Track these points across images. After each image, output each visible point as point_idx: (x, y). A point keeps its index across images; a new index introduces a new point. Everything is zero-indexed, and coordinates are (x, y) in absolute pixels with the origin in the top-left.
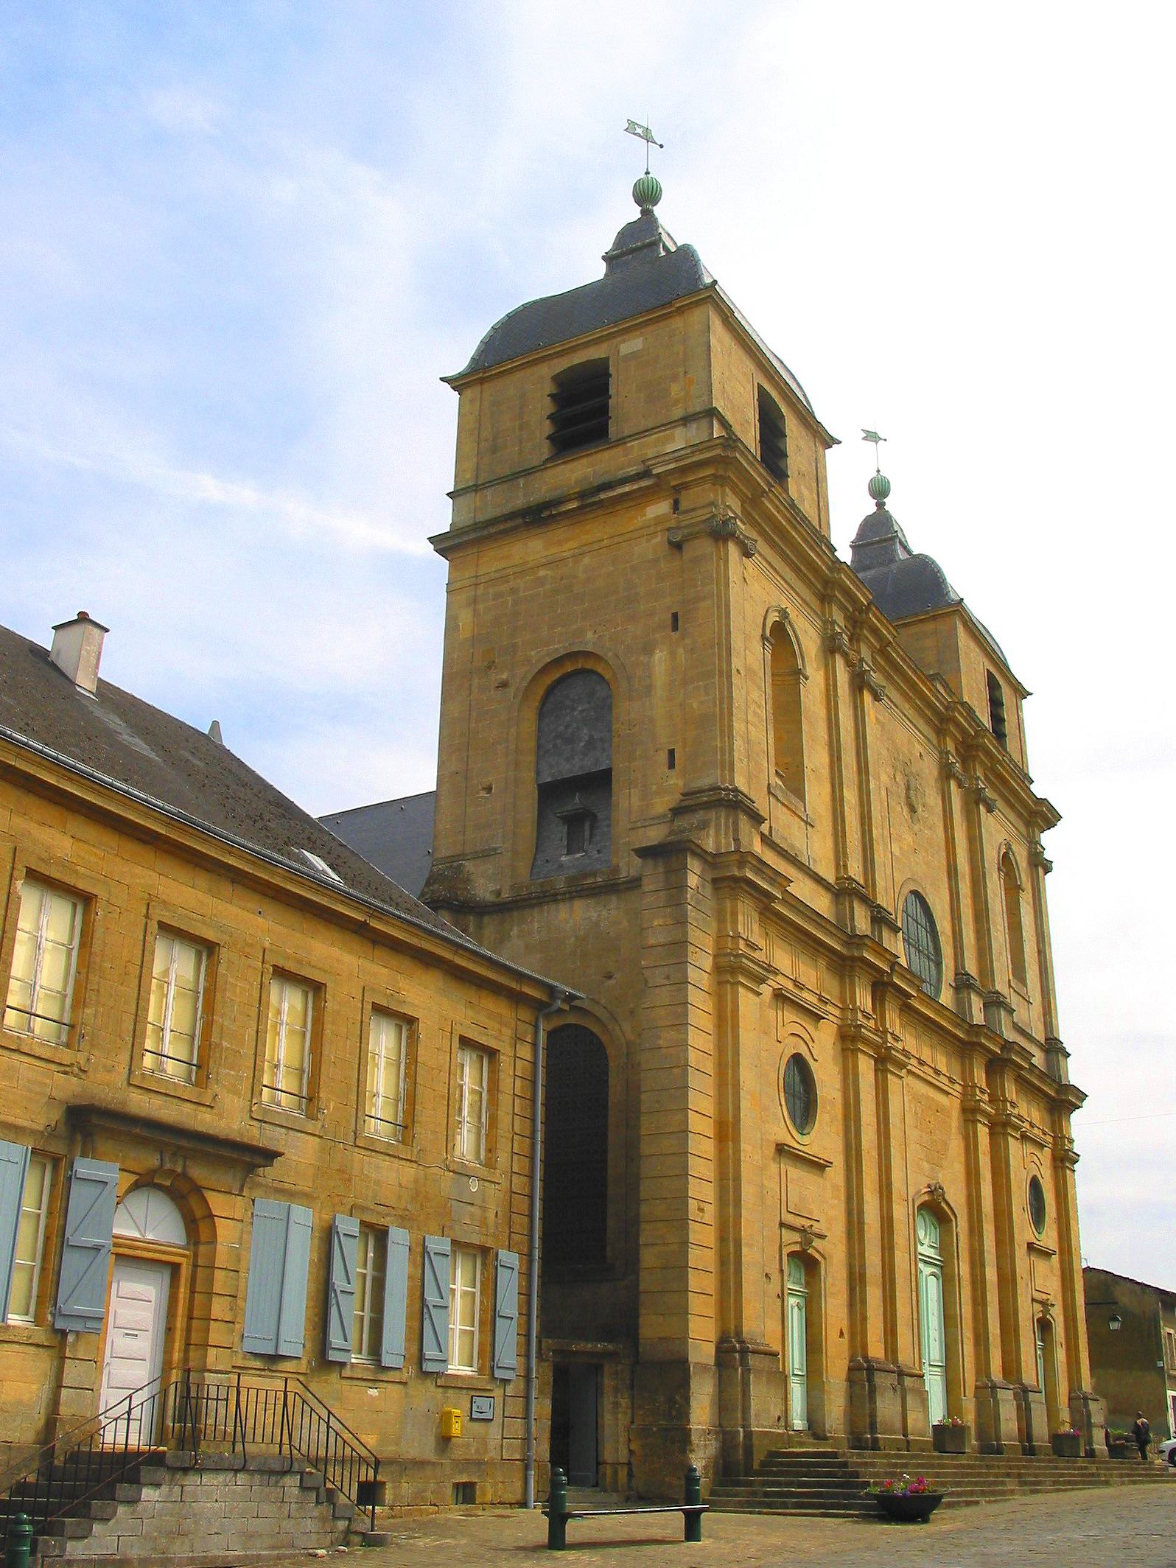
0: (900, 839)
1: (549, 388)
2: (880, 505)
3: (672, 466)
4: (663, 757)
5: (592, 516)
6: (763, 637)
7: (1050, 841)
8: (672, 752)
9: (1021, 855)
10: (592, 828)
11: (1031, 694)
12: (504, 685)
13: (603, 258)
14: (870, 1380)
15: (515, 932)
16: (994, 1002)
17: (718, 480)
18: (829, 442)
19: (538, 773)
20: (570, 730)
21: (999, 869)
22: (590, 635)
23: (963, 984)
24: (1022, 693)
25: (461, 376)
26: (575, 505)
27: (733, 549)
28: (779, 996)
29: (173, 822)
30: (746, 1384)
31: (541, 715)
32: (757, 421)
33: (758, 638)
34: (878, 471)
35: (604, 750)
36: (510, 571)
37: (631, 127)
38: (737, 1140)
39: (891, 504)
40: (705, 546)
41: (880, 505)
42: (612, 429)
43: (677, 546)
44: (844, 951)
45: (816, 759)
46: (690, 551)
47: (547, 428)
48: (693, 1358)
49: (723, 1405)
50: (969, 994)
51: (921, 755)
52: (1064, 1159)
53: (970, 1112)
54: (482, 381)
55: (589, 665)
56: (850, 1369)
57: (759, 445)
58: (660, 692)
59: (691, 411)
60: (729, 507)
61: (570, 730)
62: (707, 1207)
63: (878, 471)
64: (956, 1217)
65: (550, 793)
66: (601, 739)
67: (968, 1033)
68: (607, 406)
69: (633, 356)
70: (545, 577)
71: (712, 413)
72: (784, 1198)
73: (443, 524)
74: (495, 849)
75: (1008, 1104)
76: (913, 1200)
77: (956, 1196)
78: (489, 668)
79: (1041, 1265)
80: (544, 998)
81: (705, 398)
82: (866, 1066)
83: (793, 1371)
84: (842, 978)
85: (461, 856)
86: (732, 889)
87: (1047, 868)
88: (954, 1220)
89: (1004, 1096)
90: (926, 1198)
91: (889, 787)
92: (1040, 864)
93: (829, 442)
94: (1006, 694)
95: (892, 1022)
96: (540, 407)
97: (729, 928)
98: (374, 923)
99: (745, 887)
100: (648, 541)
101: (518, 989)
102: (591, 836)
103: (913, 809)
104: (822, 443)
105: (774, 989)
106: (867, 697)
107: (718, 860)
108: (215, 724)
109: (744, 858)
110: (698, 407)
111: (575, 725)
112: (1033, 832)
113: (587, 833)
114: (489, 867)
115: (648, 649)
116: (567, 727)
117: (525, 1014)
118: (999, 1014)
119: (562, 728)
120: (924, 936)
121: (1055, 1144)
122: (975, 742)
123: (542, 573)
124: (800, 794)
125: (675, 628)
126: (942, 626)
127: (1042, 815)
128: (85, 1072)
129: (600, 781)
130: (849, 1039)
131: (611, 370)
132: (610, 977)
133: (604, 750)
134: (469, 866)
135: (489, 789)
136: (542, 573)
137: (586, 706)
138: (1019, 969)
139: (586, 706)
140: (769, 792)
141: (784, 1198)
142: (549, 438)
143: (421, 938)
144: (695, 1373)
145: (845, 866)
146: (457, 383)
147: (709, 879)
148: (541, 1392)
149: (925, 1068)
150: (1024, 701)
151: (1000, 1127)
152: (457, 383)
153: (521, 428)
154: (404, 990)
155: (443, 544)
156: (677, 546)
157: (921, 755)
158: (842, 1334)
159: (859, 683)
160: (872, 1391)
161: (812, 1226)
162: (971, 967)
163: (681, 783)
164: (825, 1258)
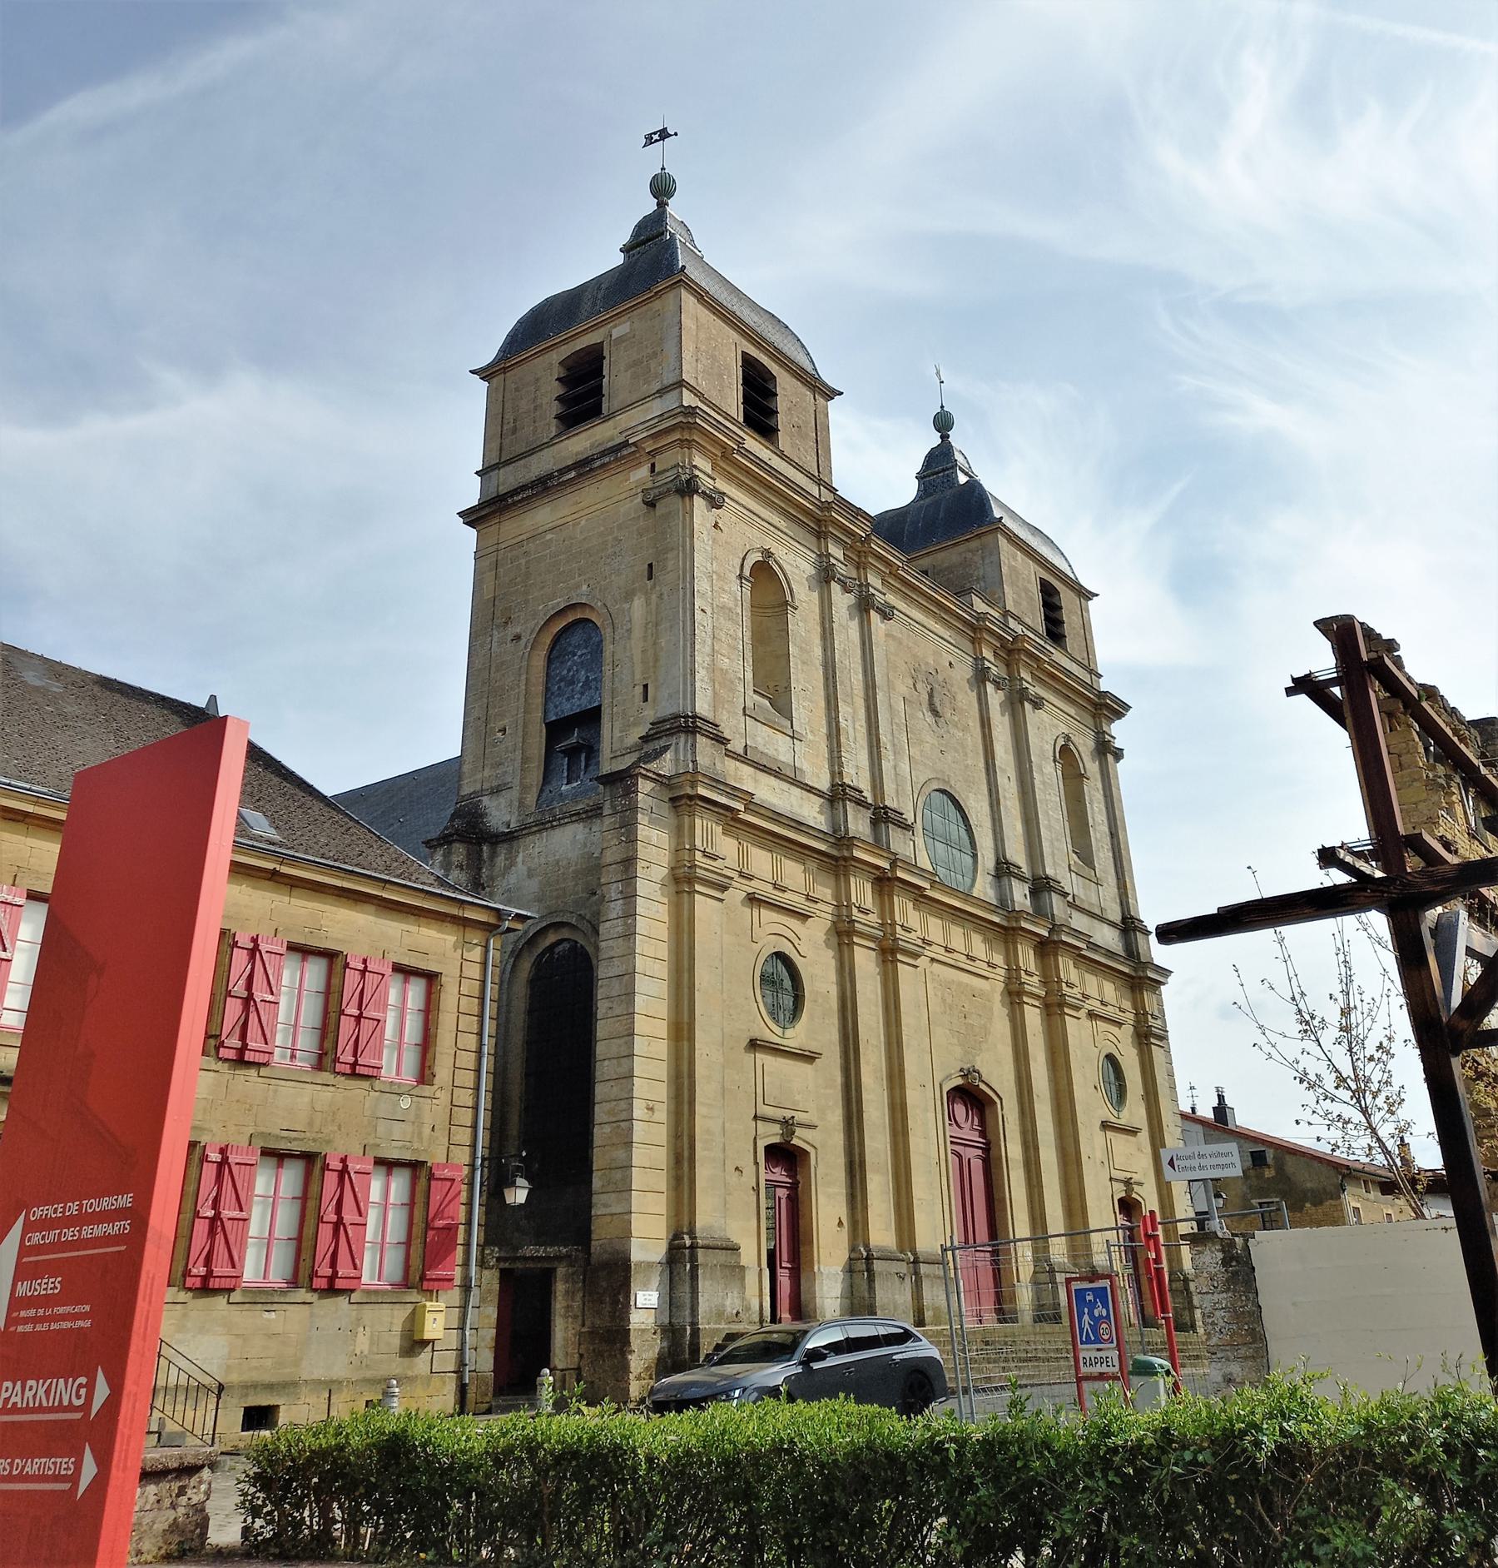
0: (921, 742)
1: (557, 372)
2: (945, 437)
3: (645, 435)
4: (639, 690)
5: (587, 484)
6: (741, 577)
7: (1120, 732)
8: (646, 687)
9: (1084, 744)
10: (587, 759)
11: (1097, 595)
12: (518, 638)
13: (621, 250)
14: (870, 1270)
15: (520, 859)
16: (1041, 886)
17: (687, 444)
18: (831, 394)
19: (546, 712)
20: (571, 673)
21: (1055, 761)
22: (585, 587)
23: (1004, 870)
24: (1086, 595)
25: (489, 366)
26: (573, 474)
27: (698, 501)
28: (753, 900)
29: (40, 800)
30: (694, 1277)
31: (550, 660)
32: (740, 386)
33: (733, 577)
34: (942, 407)
35: (597, 689)
36: (524, 537)
37: (649, 140)
38: (691, 1039)
39: (955, 438)
40: (674, 502)
41: (945, 437)
42: (605, 406)
43: (651, 505)
44: (835, 852)
45: (805, 681)
46: (661, 508)
47: (555, 408)
48: (637, 1255)
49: (671, 1301)
50: (1010, 881)
51: (950, 664)
52: (1148, 1035)
53: (1014, 994)
54: (505, 370)
55: (587, 615)
56: (1035, 1272)
57: (741, 407)
58: (637, 633)
59: (666, 383)
60: (695, 467)
61: (571, 673)
62: (657, 1106)
63: (942, 407)
64: (1001, 1099)
65: (556, 730)
66: (595, 679)
67: (1008, 918)
68: (600, 386)
69: (621, 339)
70: (551, 539)
71: (681, 384)
72: (759, 1091)
73: (472, 499)
74: (505, 784)
75: (1064, 984)
76: (941, 1085)
77: (999, 1077)
78: (507, 623)
79: (1119, 1141)
80: (492, 920)
81: (677, 371)
82: (865, 960)
83: (781, 1264)
84: (837, 876)
85: (479, 793)
86: (690, 806)
87: (1118, 754)
88: (998, 1101)
89: (1059, 977)
90: (960, 1081)
91: (907, 697)
92: (1106, 750)
93: (831, 394)
94: (1066, 598)
95: (904, 914)
96: (550, 390)
97: (686, 840)
98: (285, 870)
99: (700, 803)
100: (632, 501)
101: (461, 915)
102: (587, 766)
103: (935, 713)
104: (823, 397)
105: (749, 894)
106: (875, 616)
107: (673, 781)
108: (213, 698)
109: (694, 776)
110: (669, 379)
111: (575, 668)
112: (1101, 722)
113: (583, 764)
114: (502, 800)
115: (629, 596)
116: (569, 671)
117: (476, 937)
118: (1050, 898)
119: (565, 672)
120: (957, 831)
121: (1137, 1021)
122: (1015, 646)
123: (549, 537)
124: (784, 710)
125: (650, 578)
126: (989, 538)
127: (1107, 708)
128: (754, 1045)
129: (592, 717)
130: (843, 934)
131: (606, 353)
132: (595, 894)
133: (597, 689)
134: (486, 801)
135: (504, 730)
136: (549, 537)
137: (584, 651)
138: (1085, 855)
139: (584, 651)
140: (745, 715)
141: (759, 1091)
142: (558, 417)
143: (343, 879)
144: (704, 1278)
145: (841, 773)
146: (485, 373)
147: (667, 800)
148: (483, 1300)
149: (955, 955)
150: (1090, 602)
151: (1055, 1007)
152: (485, 373)
153: (535, 409)
154: (327, 927)
155: (471, 517)
156: (651, 505)
157: (950, 664)
158: (840, 1223)
159: (864, 605)
160: (871, 1279)
161: (793, 1117)
162: (1017, 853)
163: (652, 713)
164: (815, 1148)
